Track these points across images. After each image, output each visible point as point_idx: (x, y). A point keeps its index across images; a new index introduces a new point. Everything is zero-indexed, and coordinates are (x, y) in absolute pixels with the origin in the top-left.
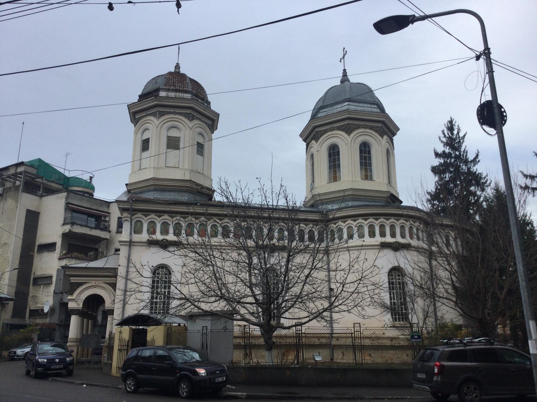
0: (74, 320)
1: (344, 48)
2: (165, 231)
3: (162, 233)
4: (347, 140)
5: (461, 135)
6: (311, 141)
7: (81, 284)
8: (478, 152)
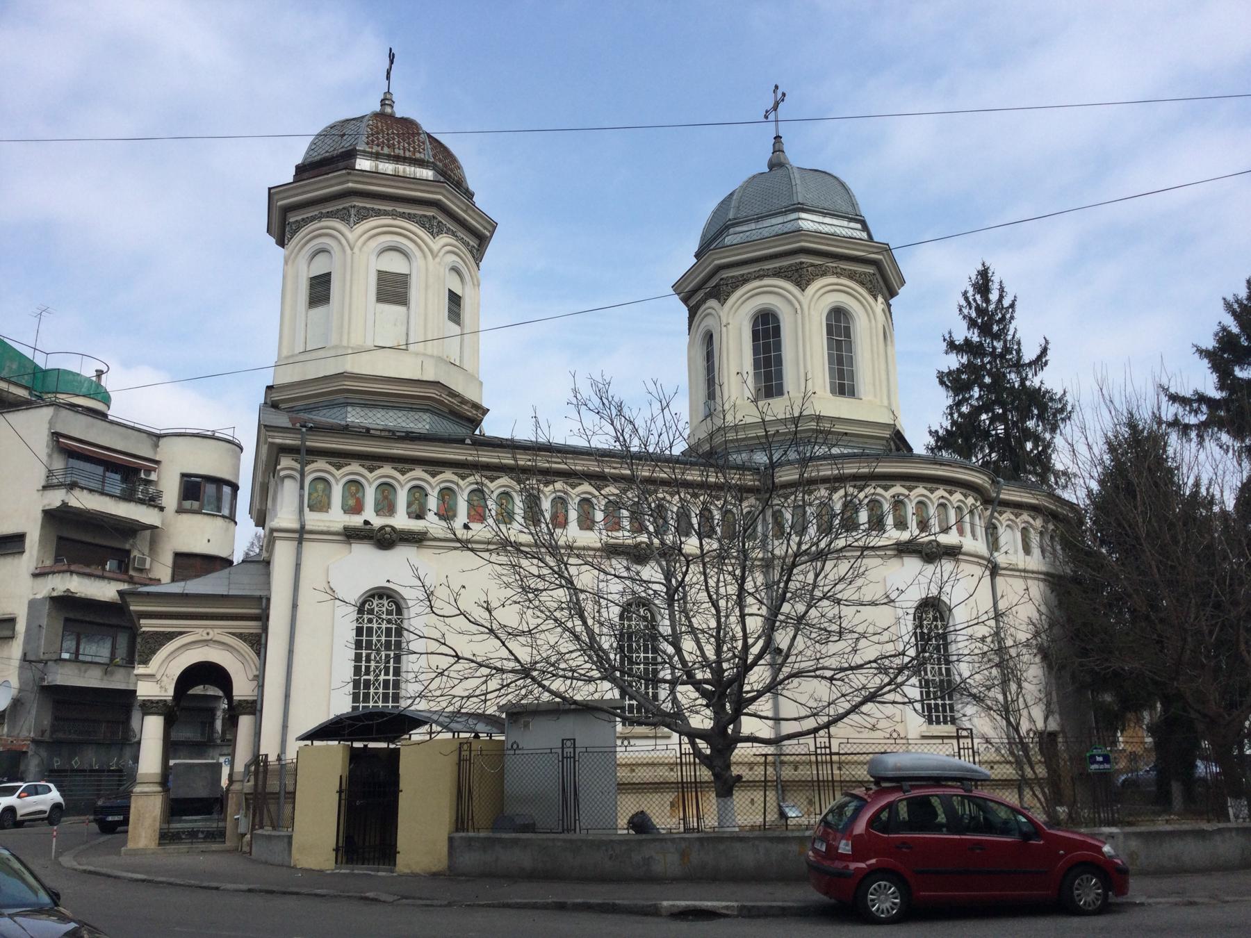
0: (152, 730)
1: (777, 87)
2: (386, 506)
3: (378, 511)
4: (799, 303)
5: (1006, 302)
6: (703, 301)
7: (170, 636)
8: (1047, 342)
